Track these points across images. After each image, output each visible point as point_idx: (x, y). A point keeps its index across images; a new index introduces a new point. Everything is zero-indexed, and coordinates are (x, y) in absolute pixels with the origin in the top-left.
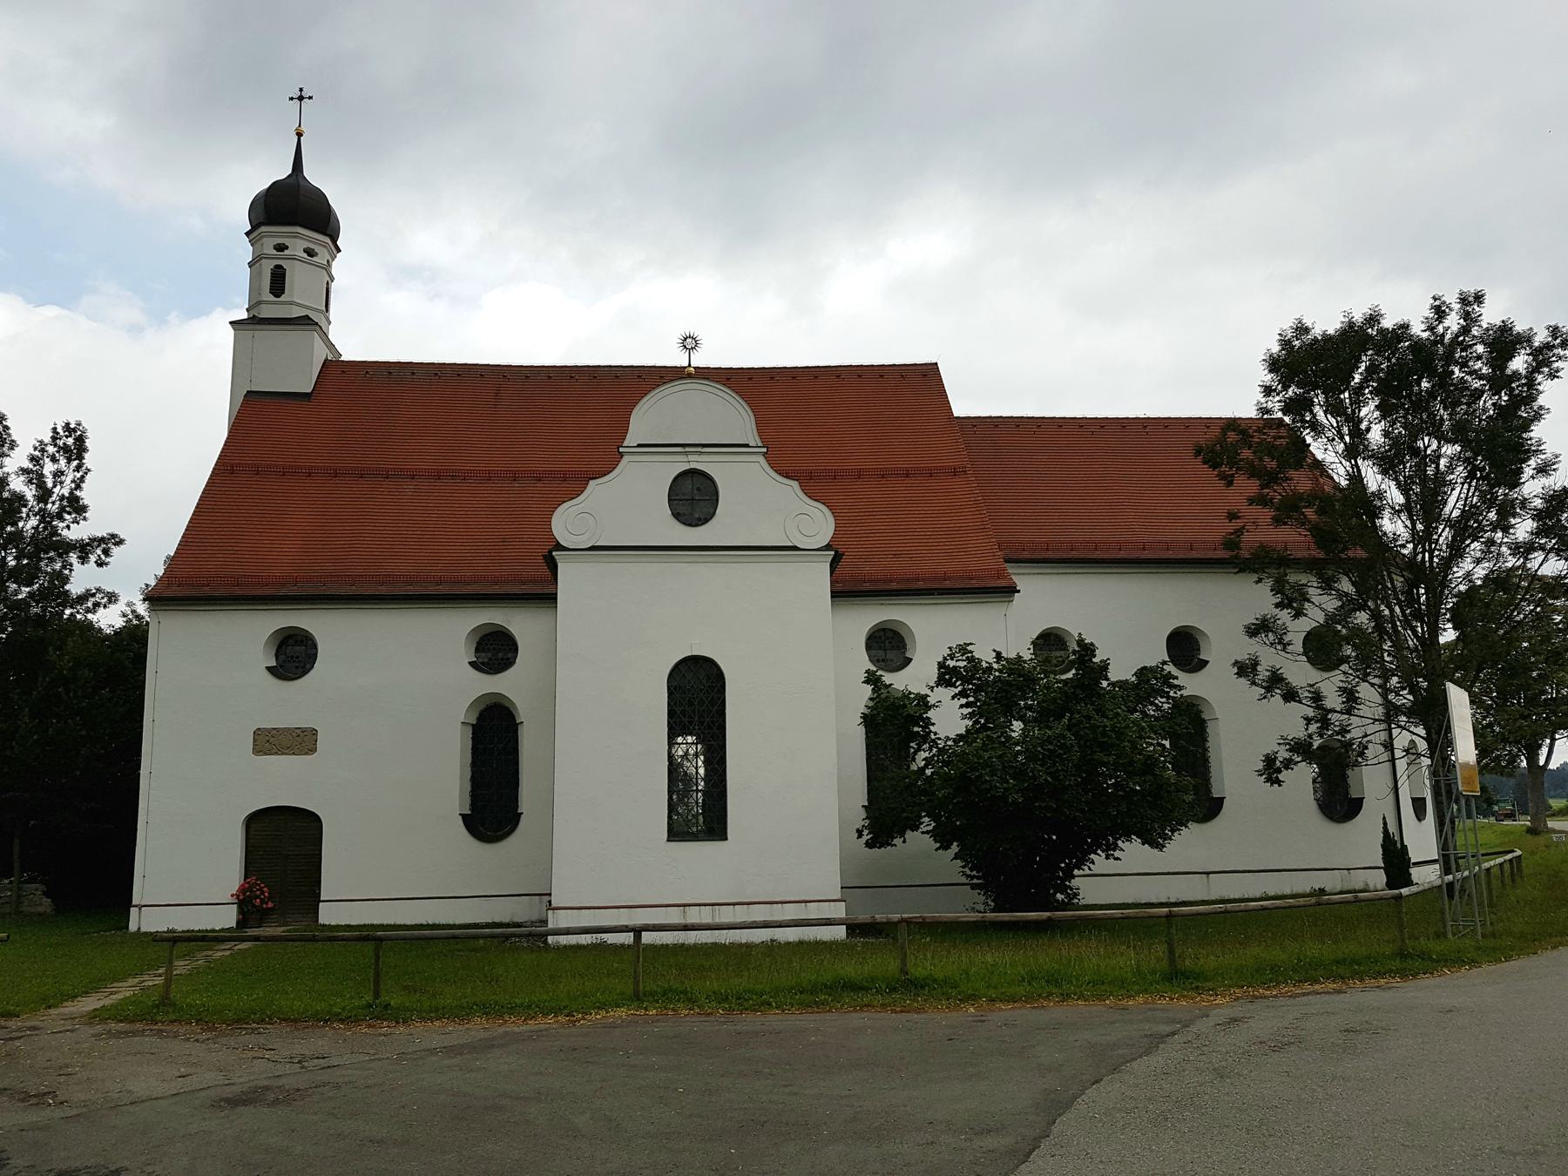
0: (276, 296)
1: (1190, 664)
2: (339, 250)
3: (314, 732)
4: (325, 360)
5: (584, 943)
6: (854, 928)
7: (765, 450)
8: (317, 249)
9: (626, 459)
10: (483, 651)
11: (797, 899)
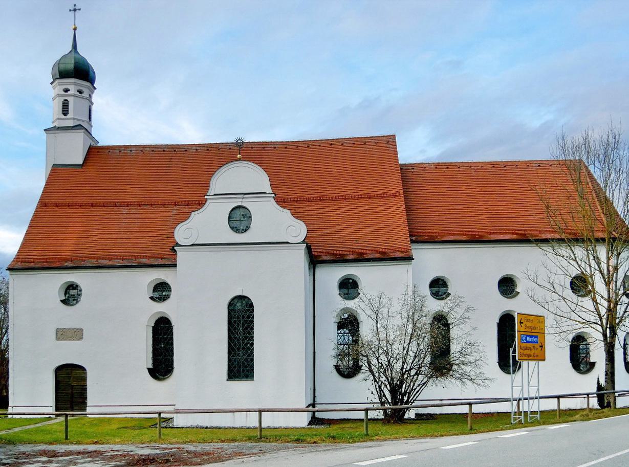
1: (511, 294)
2: (95, 88)
3: (82, 330)
4: (90, 147)
7: (273, 195)
9: (209, 201)
10: (156, 291)
11: (335, 412)
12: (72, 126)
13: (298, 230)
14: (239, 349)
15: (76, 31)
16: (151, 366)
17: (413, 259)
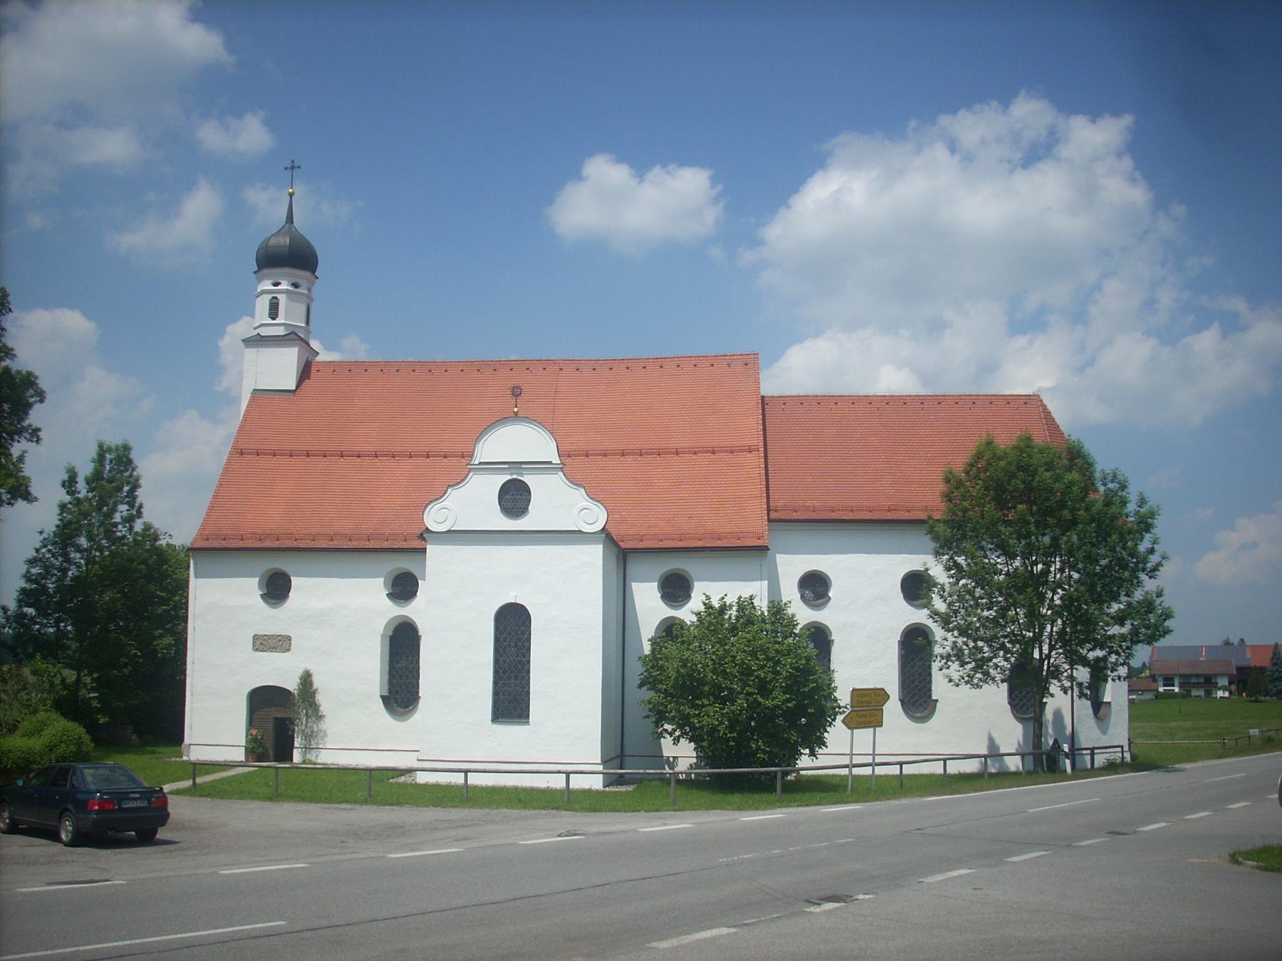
0: (276, 298)
3: (289, 638)
5: (843, 774)
6: (611, 781)
8: (300, 282)
12: (283, 334)
13: (594, 517)
14: (509, 678)
15: (293, 197)
16: (386, 694)
17: (769, 549)
